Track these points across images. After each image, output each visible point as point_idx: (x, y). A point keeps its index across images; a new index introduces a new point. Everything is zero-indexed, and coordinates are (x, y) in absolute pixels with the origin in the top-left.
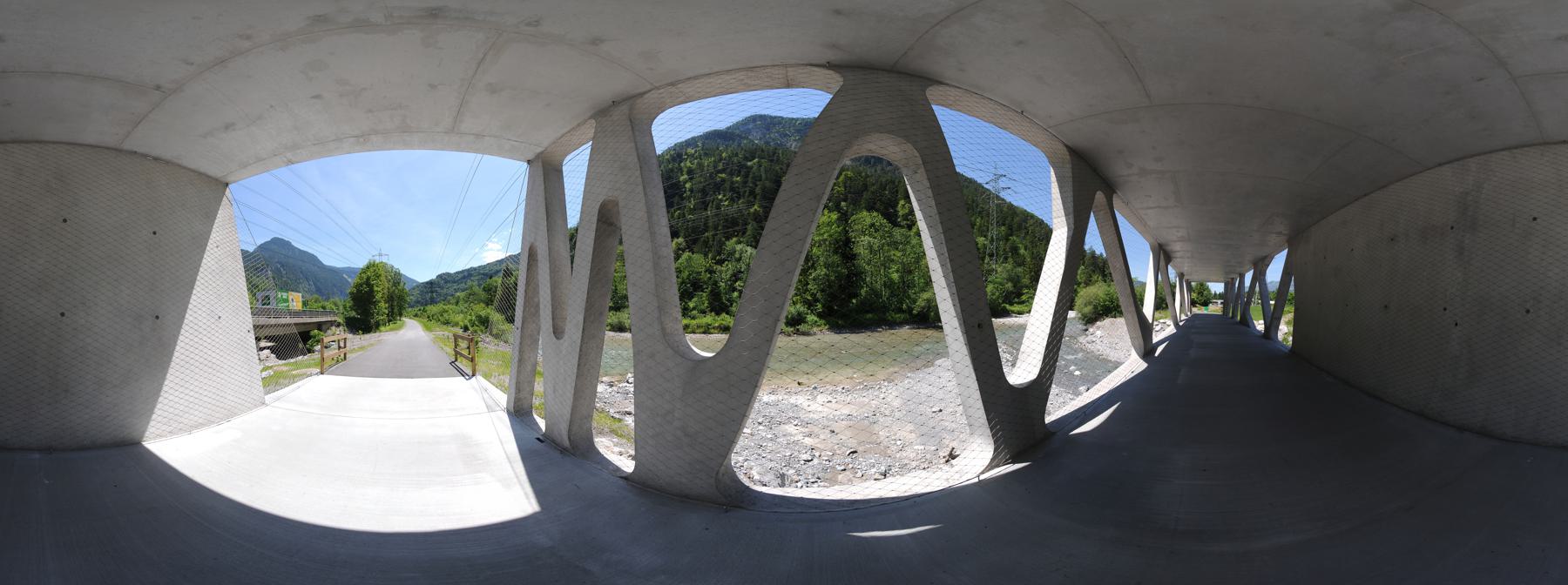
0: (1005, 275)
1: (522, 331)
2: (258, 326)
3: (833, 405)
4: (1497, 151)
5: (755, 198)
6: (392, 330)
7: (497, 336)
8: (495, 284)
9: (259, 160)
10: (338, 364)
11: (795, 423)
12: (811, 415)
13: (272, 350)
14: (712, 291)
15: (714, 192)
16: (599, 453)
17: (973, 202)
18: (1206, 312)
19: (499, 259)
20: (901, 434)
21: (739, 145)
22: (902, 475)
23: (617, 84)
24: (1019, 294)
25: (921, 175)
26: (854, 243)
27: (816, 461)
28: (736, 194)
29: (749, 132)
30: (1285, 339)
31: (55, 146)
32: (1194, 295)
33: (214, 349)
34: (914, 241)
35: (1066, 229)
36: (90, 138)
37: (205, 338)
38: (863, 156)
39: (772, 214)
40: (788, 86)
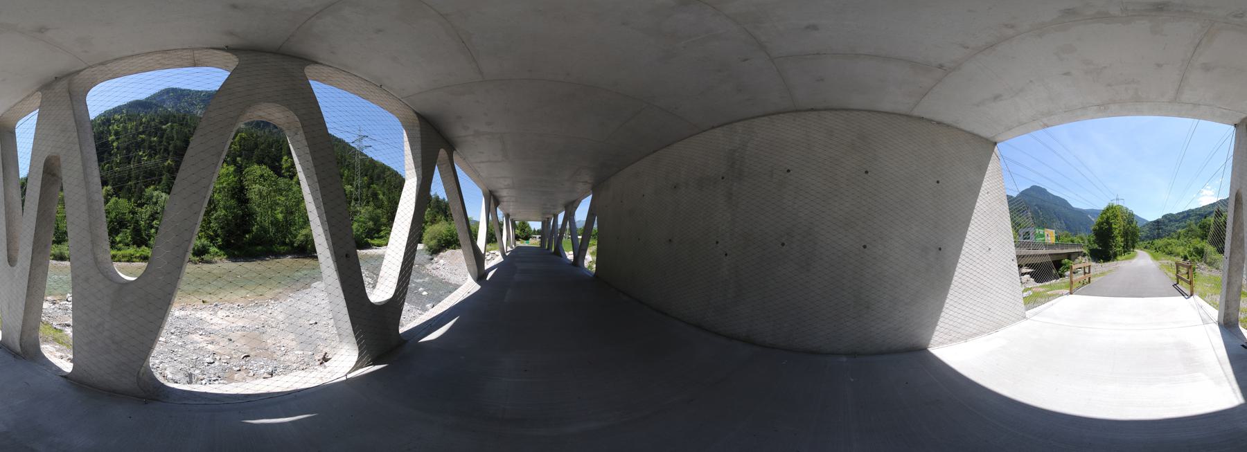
0: (367, 216)
1: (1230, 260)
2: (1020, 256)
3: (231, 319)
4: (758, 117)
5: (169, 155)
6: (1126, 259)
7: (1210, 264)
8: (1209, 223)
9: (1021, 124)
10: (1084, 286)
11: (200, 333)
12: (213, 327)
13: (1032, 275)
14: (134, 228)
15: (136, 149)
16: (44, 357)
17: (342, 157)
18: (527, 245)
19: (1212, 202)
20: (284, 342)
21: (156, 112)
22: (286, 375)
23: (59, 63)
24: (379, 231)
25: (301, 136)
26: (247, 190)
27: (217, 363)
28: (153, 151)
29: (164, 101)
30: (590, 266)
31: (870, 114)
32: (518, 232)
33: (985, 274)
34: (295, 189)
35: (416, 179)
36: (887, 107)
37: (978, 266)
38: (254, 121)
39: (182, 167)
40: (195, 65)
